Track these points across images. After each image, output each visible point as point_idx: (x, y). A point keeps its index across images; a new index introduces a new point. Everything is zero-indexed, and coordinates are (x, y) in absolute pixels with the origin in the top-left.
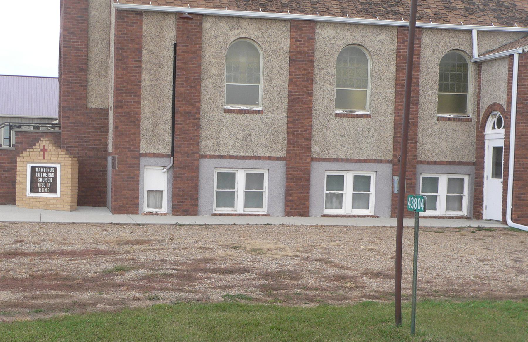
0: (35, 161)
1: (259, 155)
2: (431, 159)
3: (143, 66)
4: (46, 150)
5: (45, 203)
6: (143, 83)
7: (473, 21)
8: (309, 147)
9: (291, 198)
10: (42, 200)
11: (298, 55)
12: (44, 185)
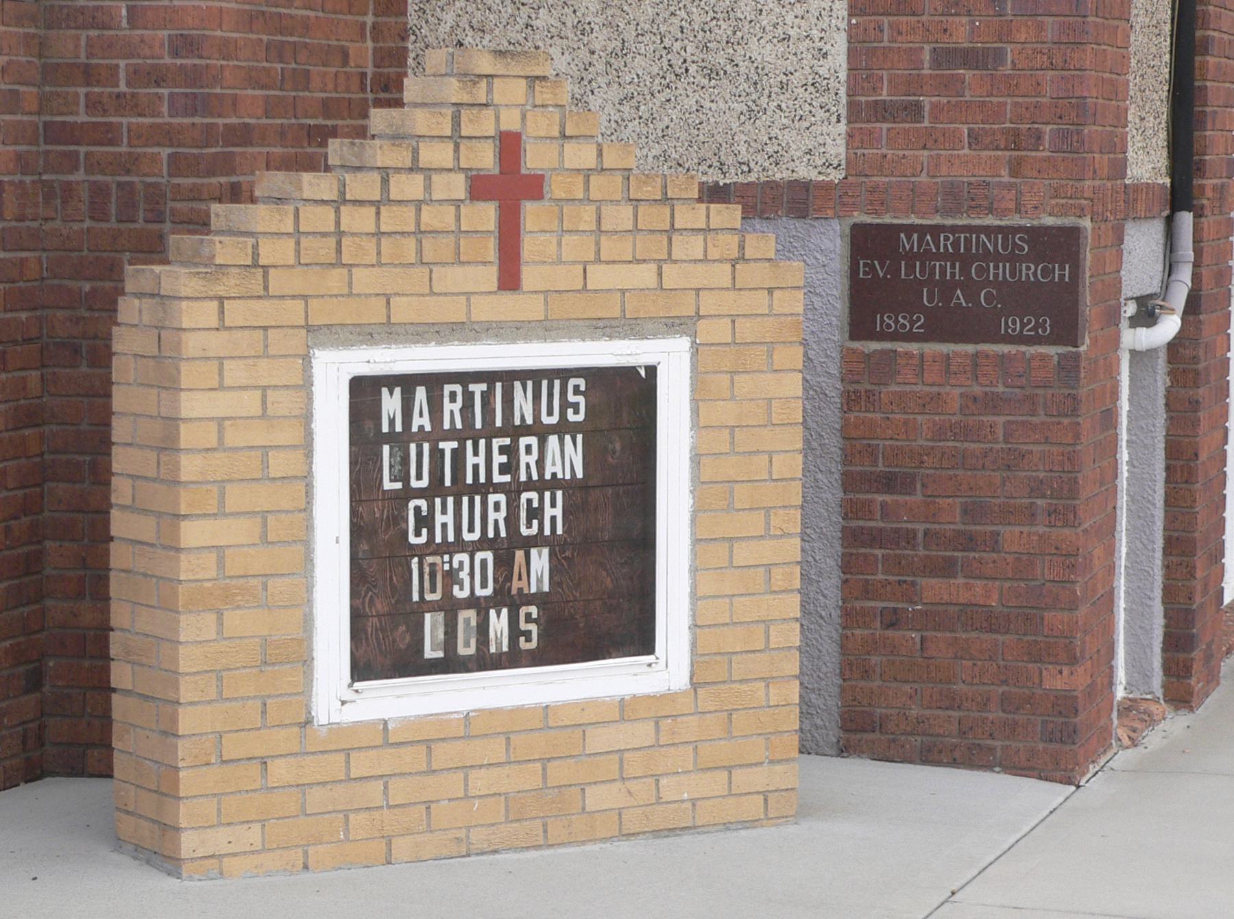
0: (403, 311)
4: (535, 187)
5: (529, 778)
10: (495, 749)
12: (473, 576)
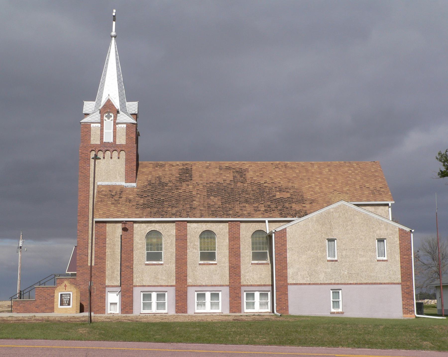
1: (162, 284)
2: (249, 284)
3: (107, 246)
6: (107, 254)
7: (266, 216)
8: (186, 280)
9: (178, 305)
11: (179, 237)
12: (65, 302)
